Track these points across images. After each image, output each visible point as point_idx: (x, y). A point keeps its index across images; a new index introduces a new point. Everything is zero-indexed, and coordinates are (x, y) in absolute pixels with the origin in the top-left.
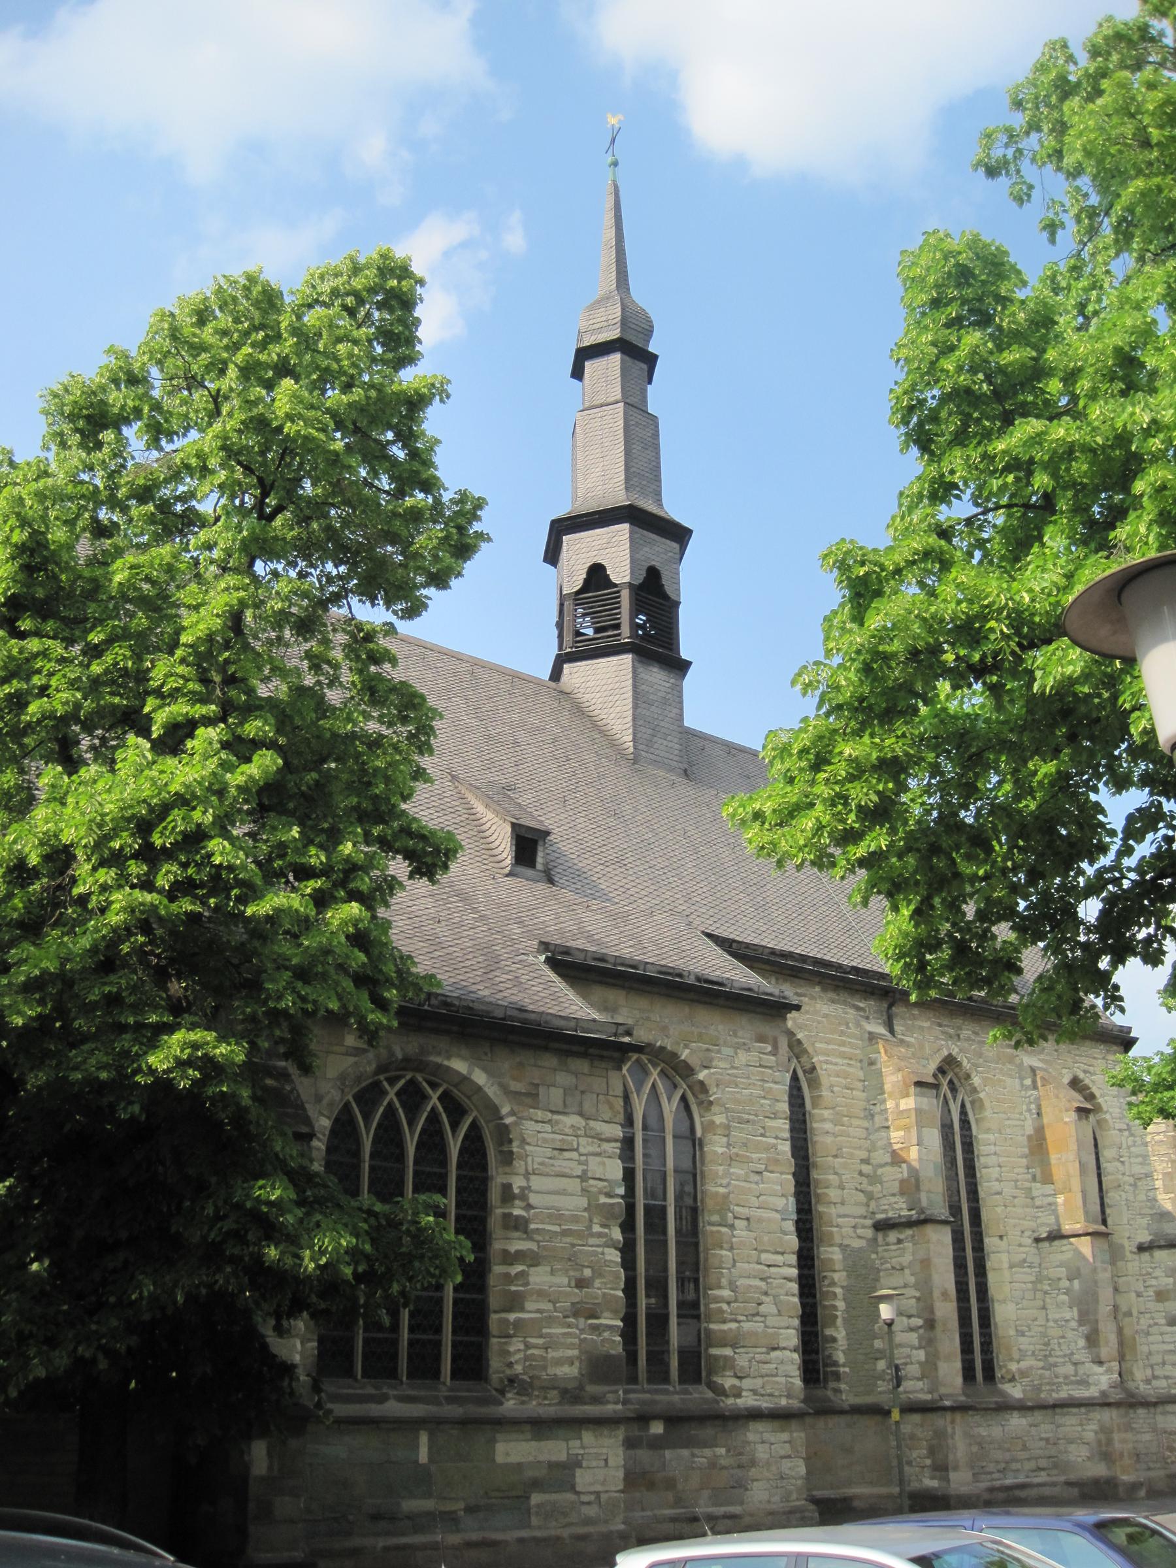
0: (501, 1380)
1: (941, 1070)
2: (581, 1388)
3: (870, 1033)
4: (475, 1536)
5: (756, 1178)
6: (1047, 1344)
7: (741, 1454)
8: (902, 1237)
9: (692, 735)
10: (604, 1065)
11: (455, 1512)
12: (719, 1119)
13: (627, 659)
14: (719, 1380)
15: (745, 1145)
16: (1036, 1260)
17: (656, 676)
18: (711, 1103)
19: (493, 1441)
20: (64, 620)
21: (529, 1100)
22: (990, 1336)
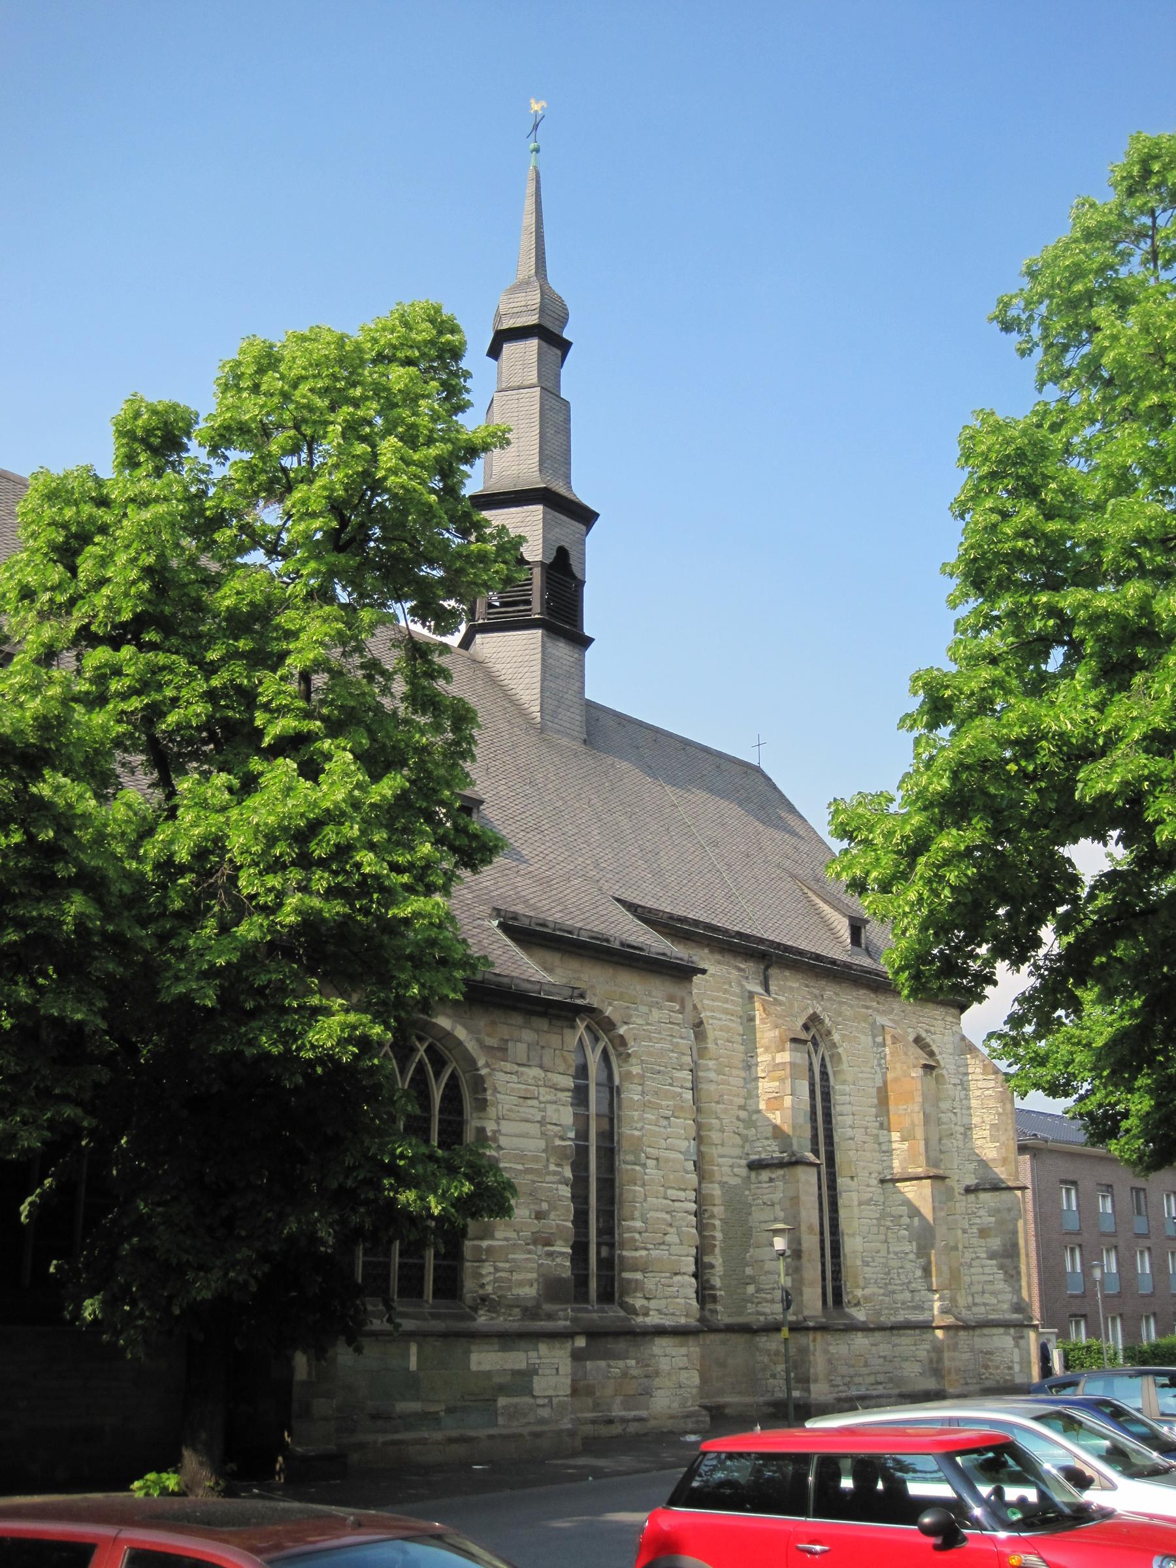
0: (474, 1299)
1: (806, 1027)
2: (538, 1306)
3: (750, 992)
4: (454, 1434)
5: (665, 1123)
6: (888, 1273)
7: (648, 1365)
8: (774, 1176)
9: (590, 705)
10: (560, 1023)
11: (437, 1413)
12: (636, 1070)
13: (538, 633)
14: (630, 1301)
15: (656, 1093)
16: (882, 1199)
17: (562, 650)
18: (629, 1055)
19: (467, 1353)
20: (184, 637)
21: (499, 1054)
22: (840, 1266)
